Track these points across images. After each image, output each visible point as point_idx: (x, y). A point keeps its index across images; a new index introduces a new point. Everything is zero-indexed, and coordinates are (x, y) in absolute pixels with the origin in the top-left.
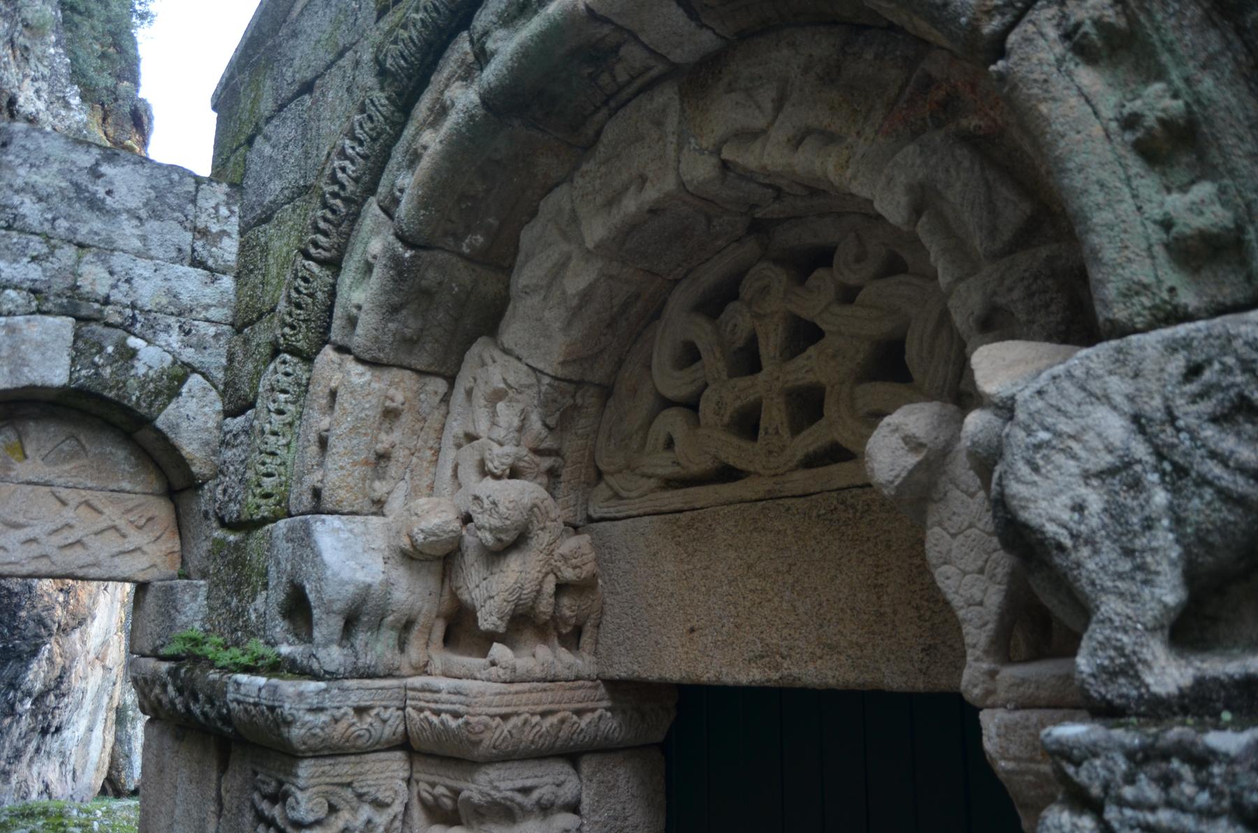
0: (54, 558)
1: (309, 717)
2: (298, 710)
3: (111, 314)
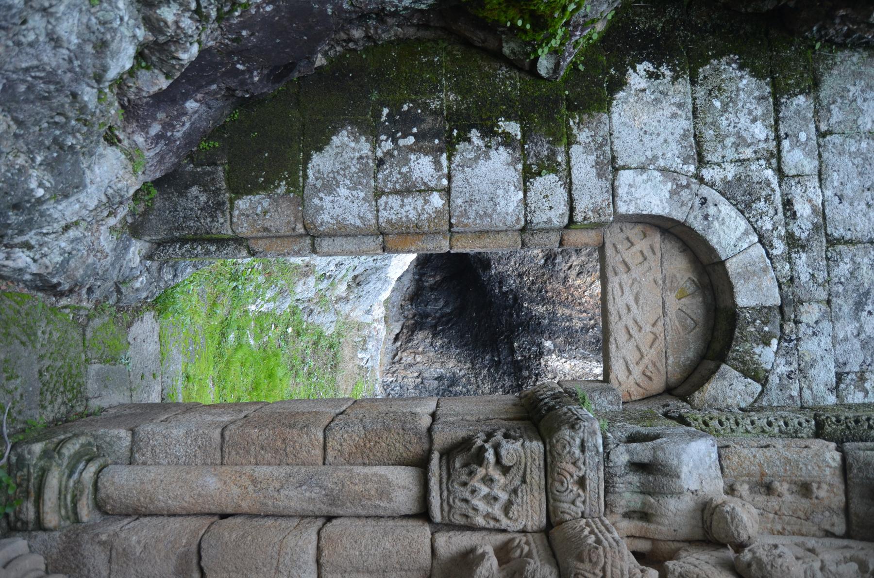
0: (619, 323)
1: (578, 441)
2: (583, 432)
3: (789, 327)
